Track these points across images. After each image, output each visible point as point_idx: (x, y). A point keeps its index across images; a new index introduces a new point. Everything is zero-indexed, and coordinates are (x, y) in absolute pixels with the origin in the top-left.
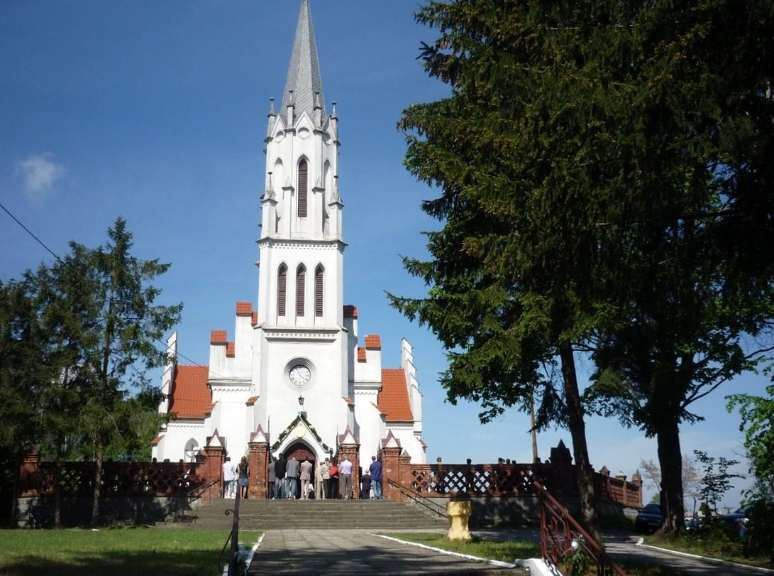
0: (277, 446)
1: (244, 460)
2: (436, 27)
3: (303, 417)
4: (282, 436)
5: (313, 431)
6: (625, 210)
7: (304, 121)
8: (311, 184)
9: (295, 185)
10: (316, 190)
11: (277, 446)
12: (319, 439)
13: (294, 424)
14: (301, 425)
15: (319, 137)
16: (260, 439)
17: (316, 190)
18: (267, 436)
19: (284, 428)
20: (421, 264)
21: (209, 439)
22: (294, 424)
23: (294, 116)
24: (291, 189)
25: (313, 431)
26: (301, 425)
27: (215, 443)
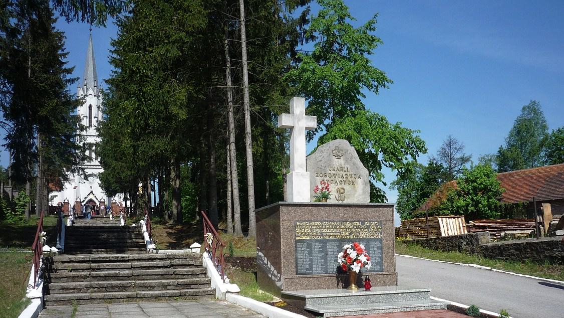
0: (83, 201)
1: (74, 205)
2: (83, 20)
3: (92, 192)
4: (85, 198)
5: (95, 196)
6: (483, 214)
7: (91, 91)
8: (93, 115)
9: (88, 116)
10: (95, 117)
11: (83, 201)
12: (97, 199)
13: (89, 194)
14: (91, 195)
15: (96, 98)
16: (78, 200)
17: (95, 117)
18: (80, 199)
19: (86, 196)
20: (340, 137)
21: (64, 200)
22: (89, 194)
23: (87, 89)
24: (87, 117)
25: (95, 196)
26: (91, 195)
27: (66, 201)
